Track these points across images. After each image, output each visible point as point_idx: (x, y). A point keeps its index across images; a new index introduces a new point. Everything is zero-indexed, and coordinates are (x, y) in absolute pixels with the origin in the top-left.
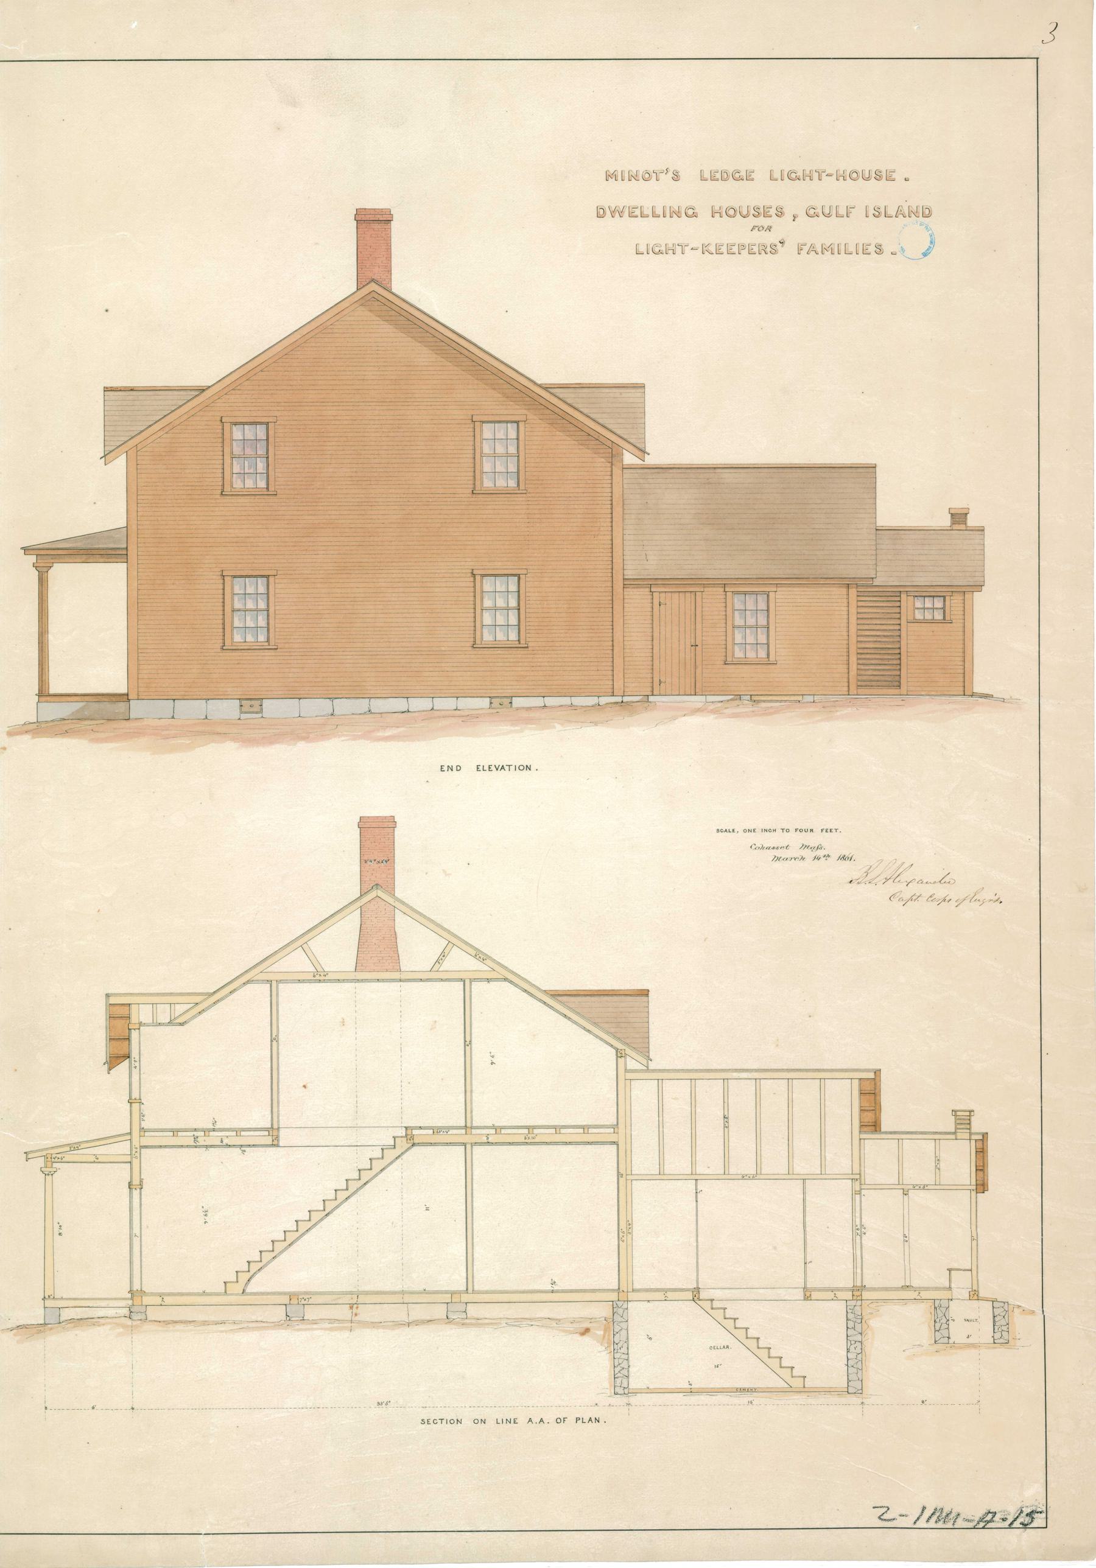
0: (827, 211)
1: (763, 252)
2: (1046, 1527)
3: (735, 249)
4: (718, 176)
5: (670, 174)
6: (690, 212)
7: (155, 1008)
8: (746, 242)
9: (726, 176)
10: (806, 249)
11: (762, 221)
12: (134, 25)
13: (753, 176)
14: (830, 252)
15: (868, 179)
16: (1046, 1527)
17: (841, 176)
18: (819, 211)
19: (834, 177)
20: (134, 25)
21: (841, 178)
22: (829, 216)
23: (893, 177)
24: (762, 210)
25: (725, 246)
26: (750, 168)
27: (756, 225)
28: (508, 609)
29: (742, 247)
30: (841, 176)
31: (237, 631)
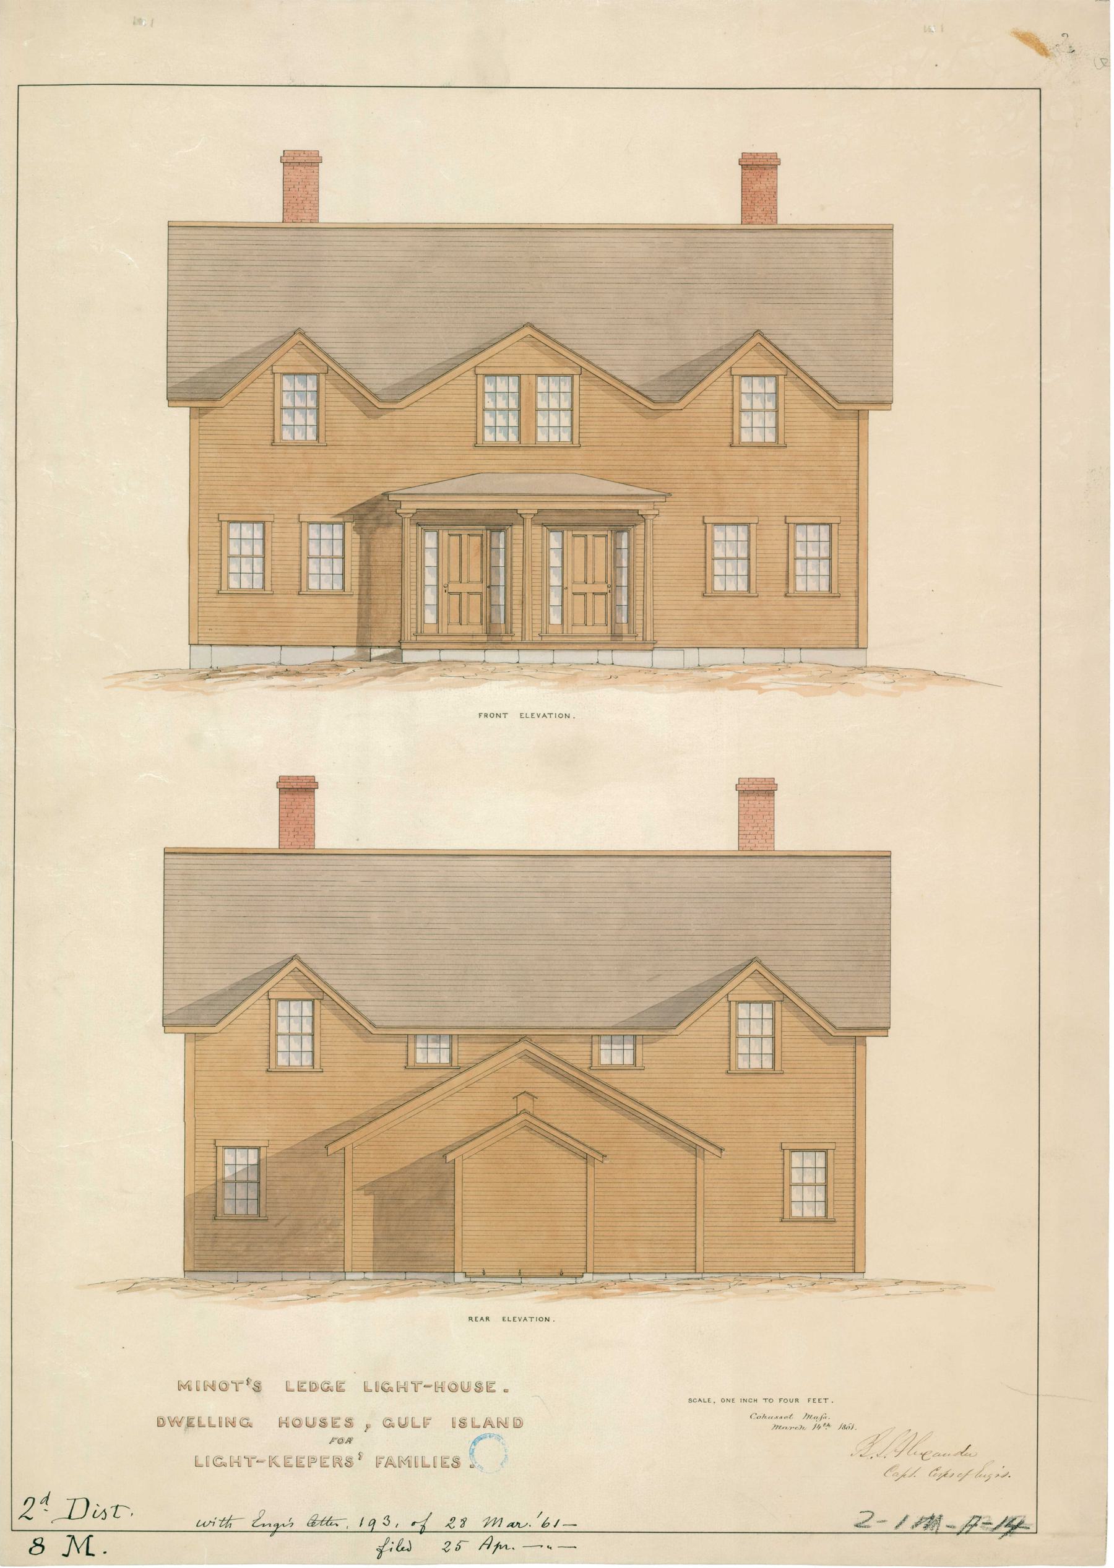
0: (403, 1422)
1: (338, 1465)
2: (1040, 89)
3: (305, 1462)
4: (307, 1386)
5: (252, 1385)
6: (245, 1422)
7: (199, 1150)
8: (318, 1454)
9: (162, 1423)
10: (384, 1461)
11: (342, 1432)
12: (26, 44)
13: (343, 1386)
14: (407, 1465)
15: (456, 1391)
16: (1040, 89)
17: (439, 1388)
18: (396, 1422)
19: (433, 1387)
20: (26, 44)
21: (284, 1425)
22: (402, 1426)
23: (337, 1424)
24: (484, 1386)
25: (306, 1458)
26: (341, 1379)
27: (335, 1437)
28: (332, 557)
29: (312, 1460)
30: (439, 1388)
31: (229, 1168)
